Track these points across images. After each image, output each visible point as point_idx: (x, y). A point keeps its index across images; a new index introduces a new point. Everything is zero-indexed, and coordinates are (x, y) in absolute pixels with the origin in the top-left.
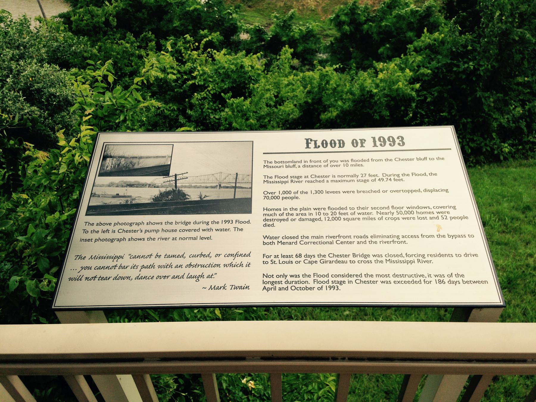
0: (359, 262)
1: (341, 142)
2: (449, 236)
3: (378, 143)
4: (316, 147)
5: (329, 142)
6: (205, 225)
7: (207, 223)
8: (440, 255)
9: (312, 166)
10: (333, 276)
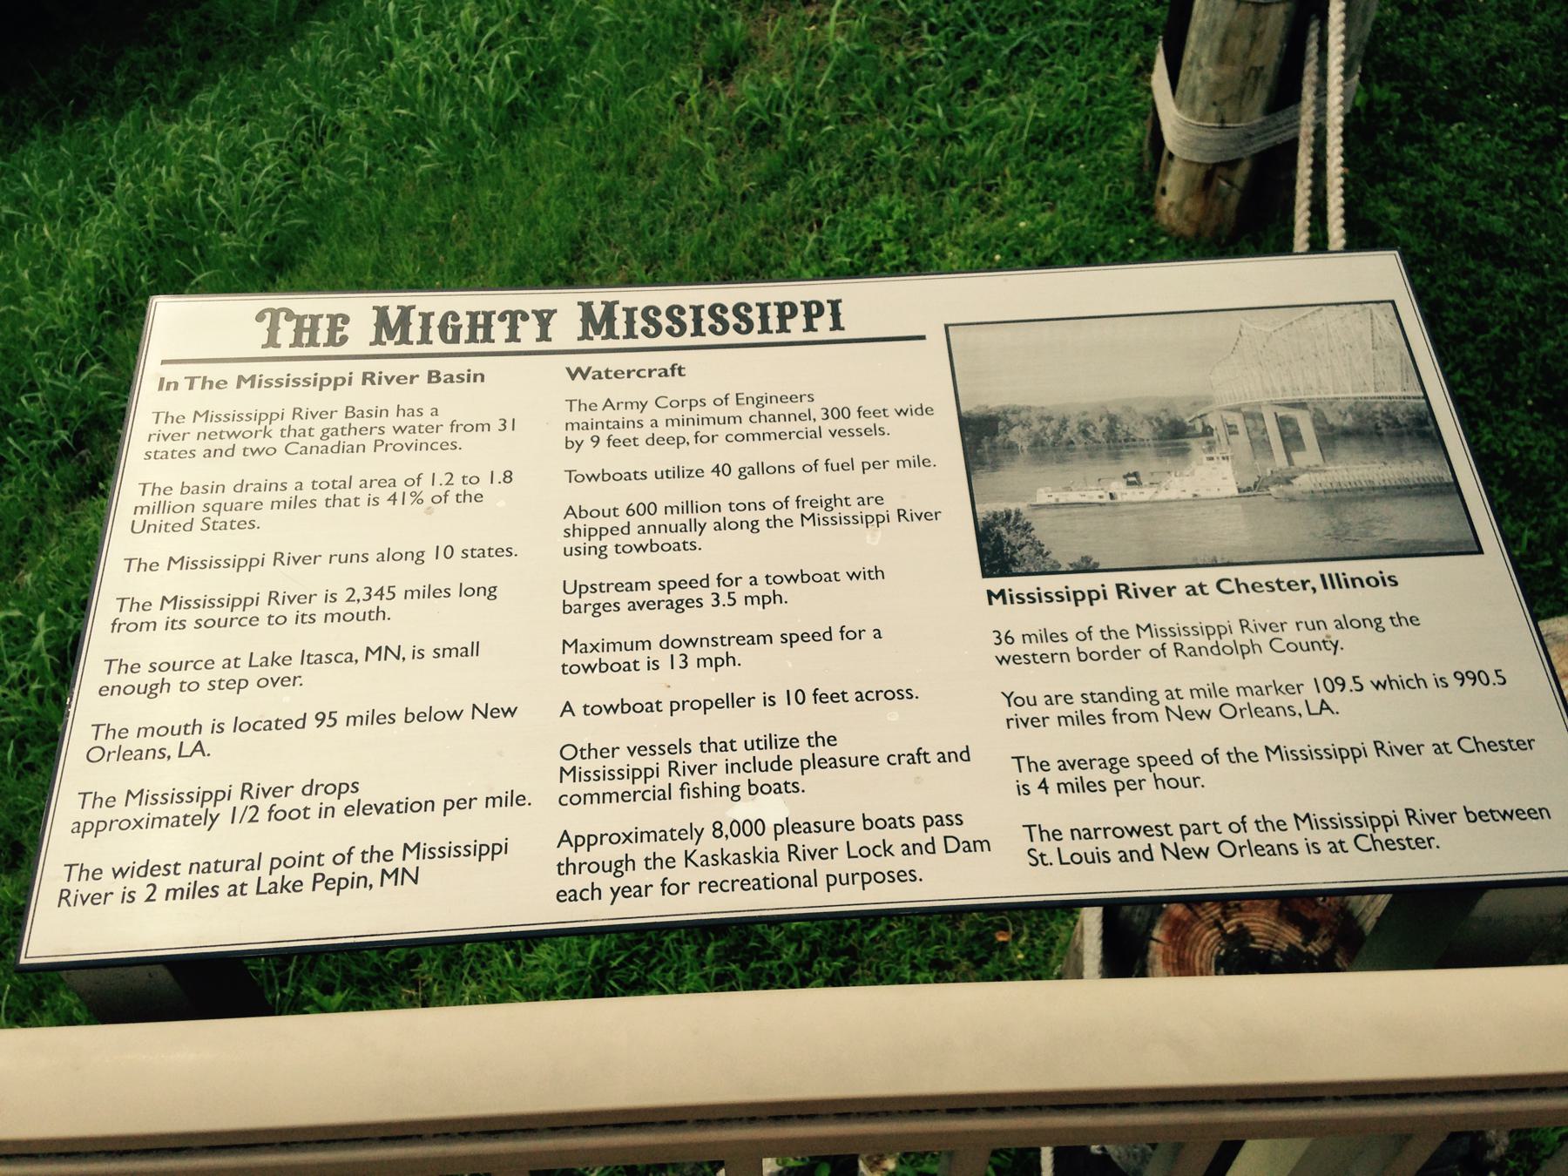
0: (893, 760)
2: (570, 445)
8: (803, 577)
9: (762, 437)
10: (564, 800)
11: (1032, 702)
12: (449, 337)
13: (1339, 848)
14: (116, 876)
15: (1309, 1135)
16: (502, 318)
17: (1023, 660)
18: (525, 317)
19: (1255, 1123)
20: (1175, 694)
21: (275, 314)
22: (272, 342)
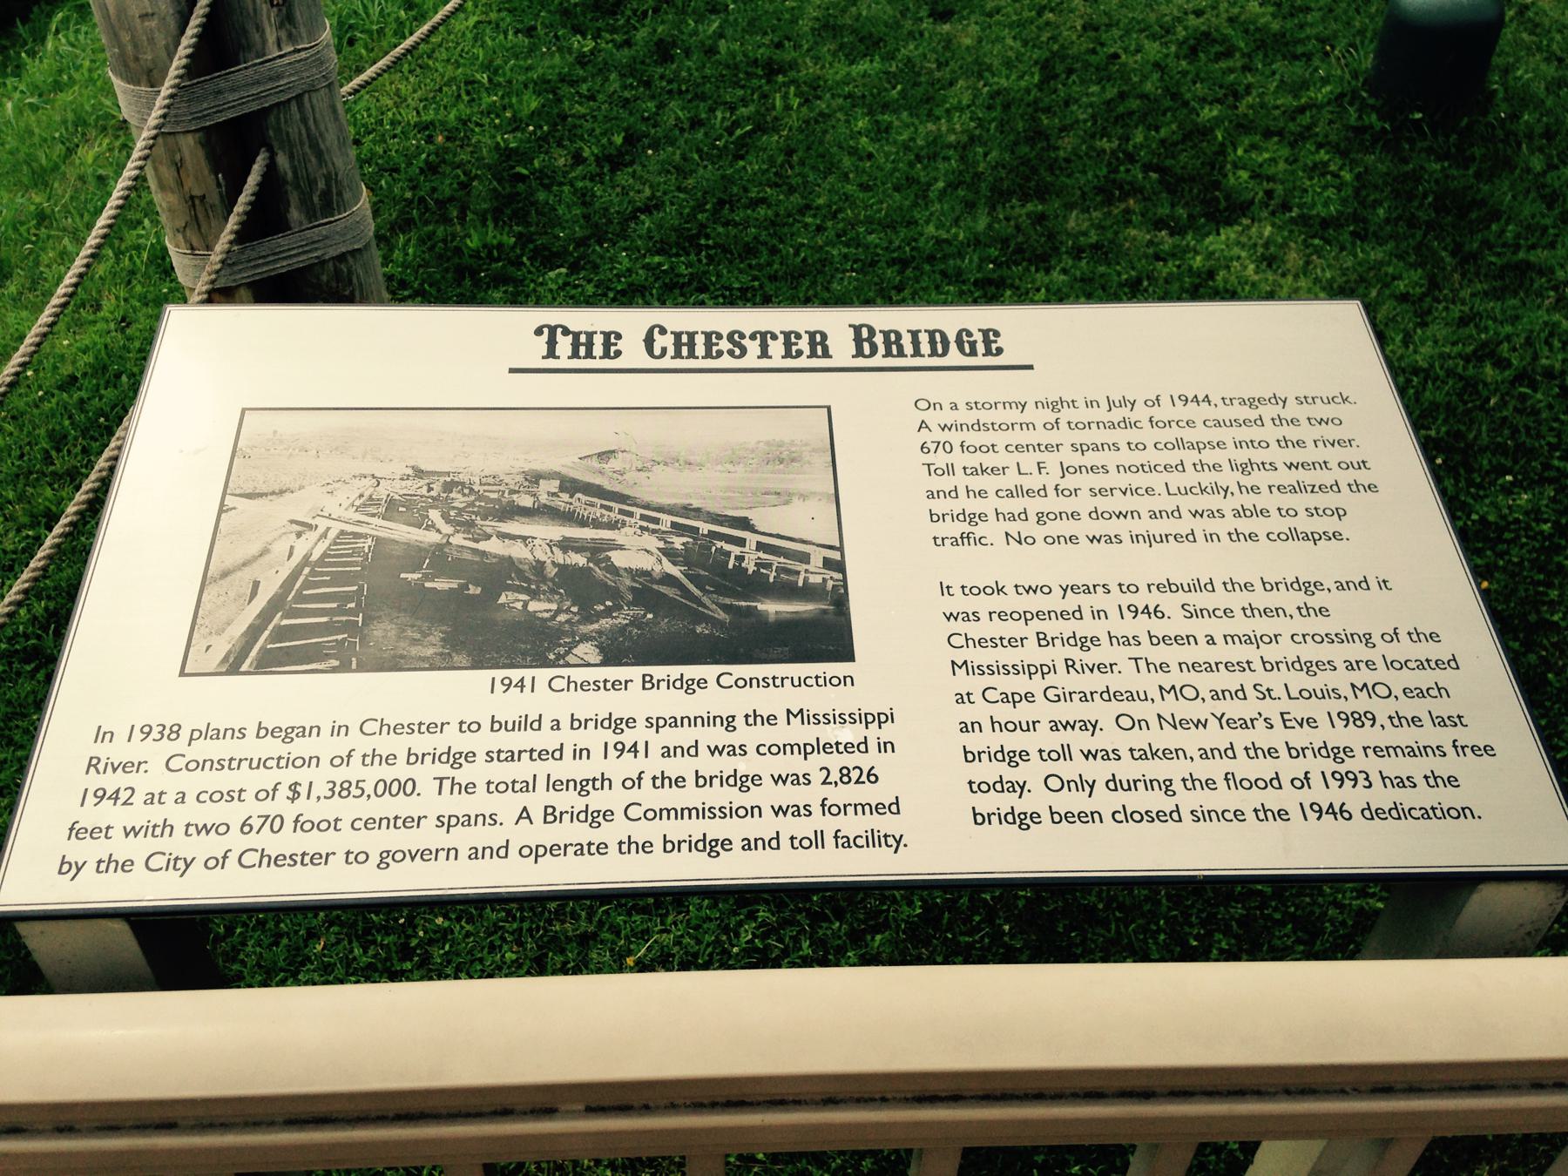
1: (938, 336)
3: (925, 348)
4: (788, 355)
5: (952, 337)
6: (719, 729)
7: (729, 723)
10: (762, 750)
11: (1184, 666)
12: (967, 350)
13: (1432, 815)
14: (127, 835)
15: (1321, 1137)
16: (753, 337)
17: (990, 643)
18: (774, 337)
19: (1281, 1118)
20: (965, 698)
21: (553, 330)
22: (551, 353)
